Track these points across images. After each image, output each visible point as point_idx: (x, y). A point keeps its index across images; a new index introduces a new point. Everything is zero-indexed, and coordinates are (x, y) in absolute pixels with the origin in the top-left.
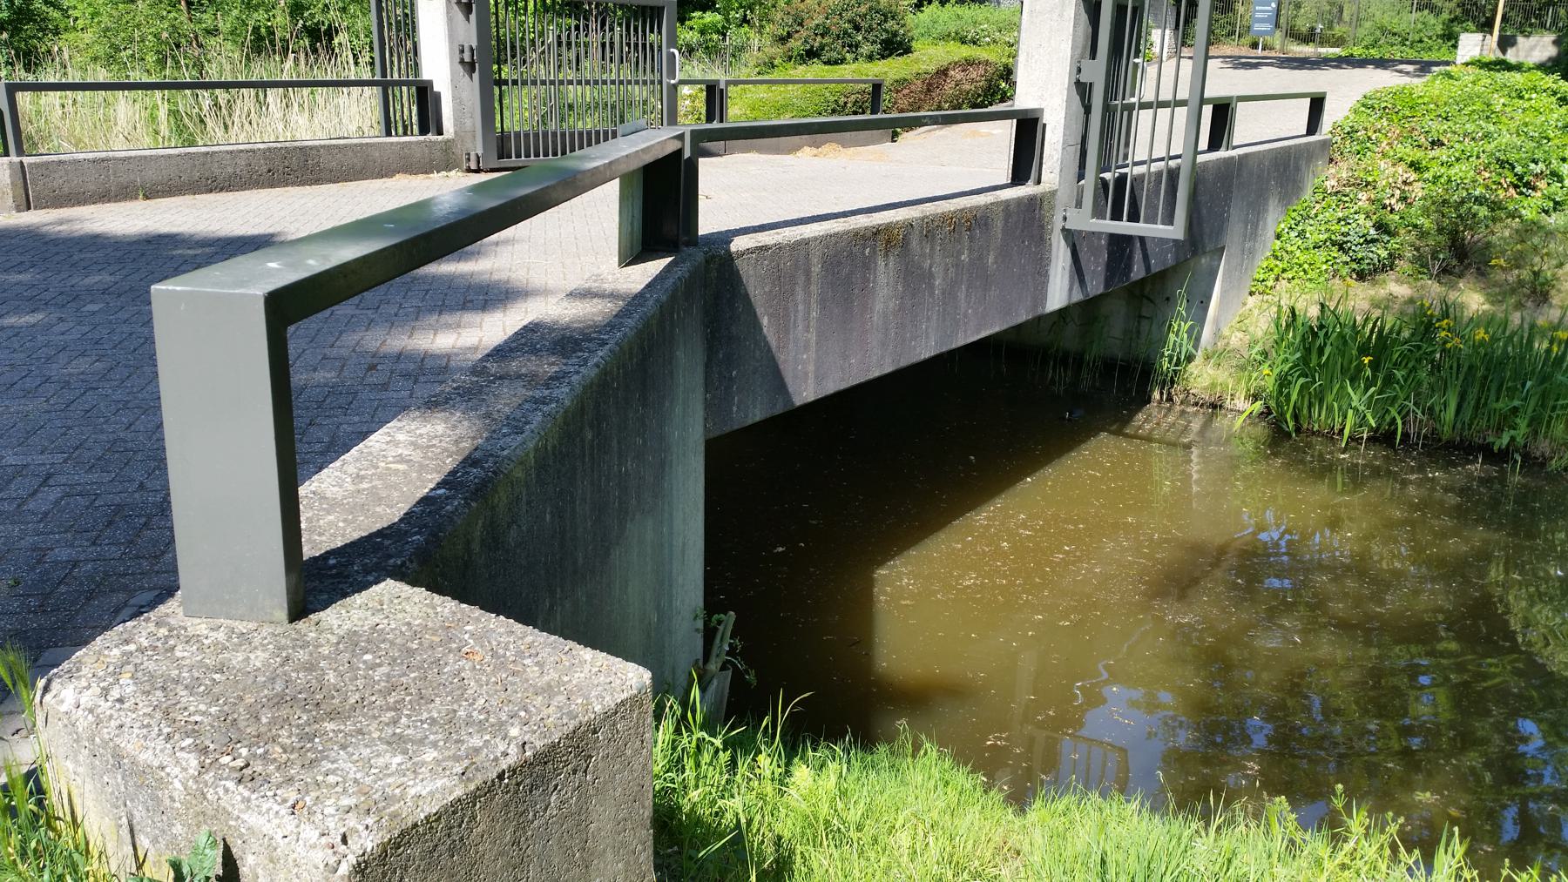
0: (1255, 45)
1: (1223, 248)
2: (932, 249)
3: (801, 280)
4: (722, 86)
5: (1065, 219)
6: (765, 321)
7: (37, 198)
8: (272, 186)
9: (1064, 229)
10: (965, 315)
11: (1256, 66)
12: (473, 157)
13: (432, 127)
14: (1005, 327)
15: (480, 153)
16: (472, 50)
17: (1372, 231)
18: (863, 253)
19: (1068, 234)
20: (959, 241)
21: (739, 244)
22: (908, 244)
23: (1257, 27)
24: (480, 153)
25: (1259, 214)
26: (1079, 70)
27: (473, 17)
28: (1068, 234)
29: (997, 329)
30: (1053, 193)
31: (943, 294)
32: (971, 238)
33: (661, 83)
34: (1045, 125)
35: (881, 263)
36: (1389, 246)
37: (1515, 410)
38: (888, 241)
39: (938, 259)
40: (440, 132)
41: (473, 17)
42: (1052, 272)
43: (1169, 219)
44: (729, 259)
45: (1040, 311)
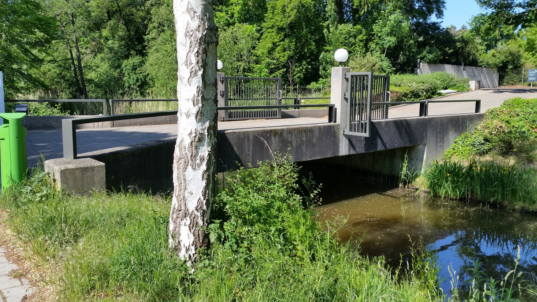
0: (530, 85)
1: (426, 144)
2: (291, 136)
3: (246, 140)
4: (299, 99)
5: (344, 132)
6: (235, 148)
7: (115, 125)
8: (170, 124)
9: (344, 134)
10: (306, 153)
11: (502, 92)
12: (222, 118)
13: (333, 120)
14: (322, 157)
15: (224, 116)
16: (223, 92)
17: (483, 141)
18: (267, 136)
19: (346, 136)
20: (302, 135)
21: (226, 132)
22: (282, 134)
23: (530, 79)
24: (224, 116)
25: (444, 135)
26: (345, 95)
27: (224, 84)
28: (346, 136)
29: (319, 158)
30: (339, 125)
31: (297, 147)
32: (306, 134)
33: (277, 99)
34: (336, 109)
35: (273, 138)
36: (489, 145)
37: (495, 191)
38: (275, 133)
39: (294, 138)
40: (335, 122)
41: (224, 84)
42: (340, 145)
43: (365, 132)
44: (224, 134)
45: (337, 155)
